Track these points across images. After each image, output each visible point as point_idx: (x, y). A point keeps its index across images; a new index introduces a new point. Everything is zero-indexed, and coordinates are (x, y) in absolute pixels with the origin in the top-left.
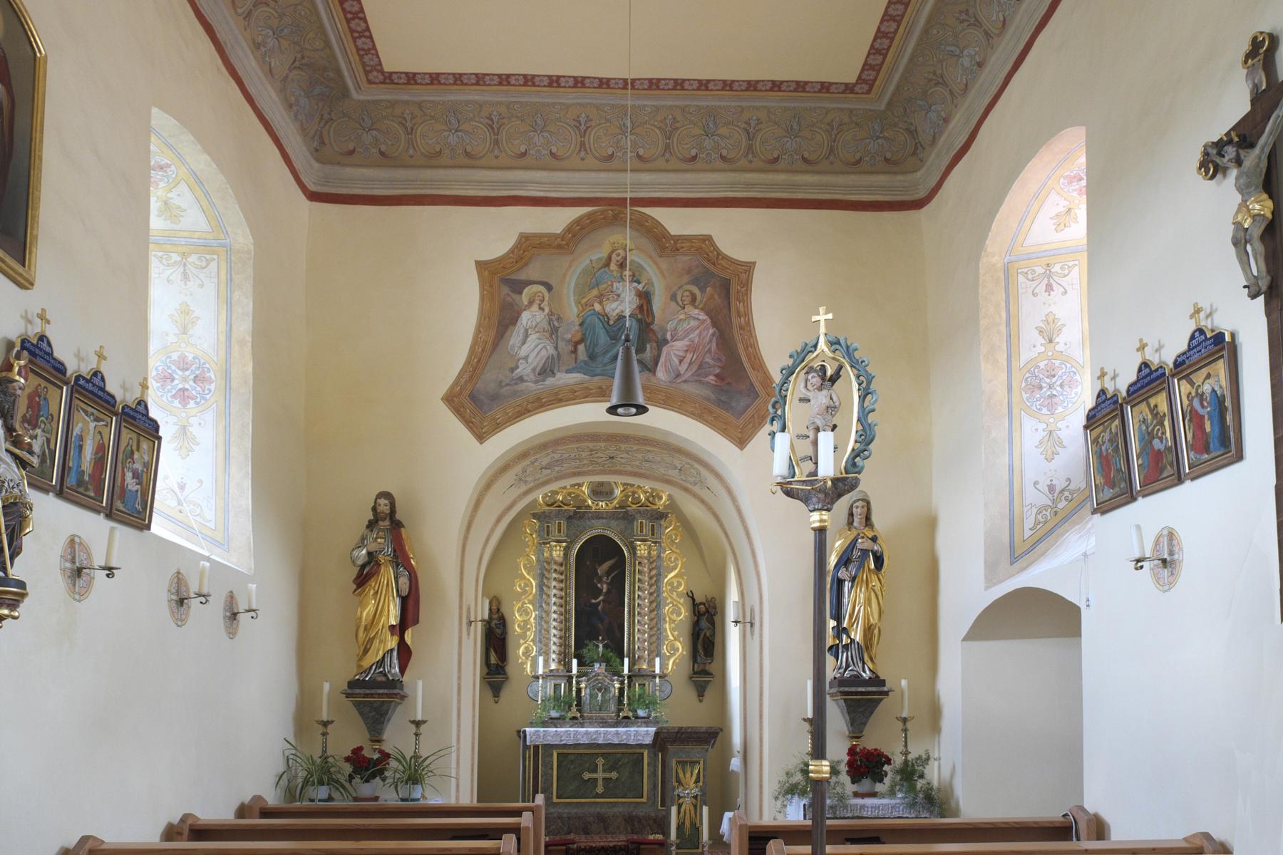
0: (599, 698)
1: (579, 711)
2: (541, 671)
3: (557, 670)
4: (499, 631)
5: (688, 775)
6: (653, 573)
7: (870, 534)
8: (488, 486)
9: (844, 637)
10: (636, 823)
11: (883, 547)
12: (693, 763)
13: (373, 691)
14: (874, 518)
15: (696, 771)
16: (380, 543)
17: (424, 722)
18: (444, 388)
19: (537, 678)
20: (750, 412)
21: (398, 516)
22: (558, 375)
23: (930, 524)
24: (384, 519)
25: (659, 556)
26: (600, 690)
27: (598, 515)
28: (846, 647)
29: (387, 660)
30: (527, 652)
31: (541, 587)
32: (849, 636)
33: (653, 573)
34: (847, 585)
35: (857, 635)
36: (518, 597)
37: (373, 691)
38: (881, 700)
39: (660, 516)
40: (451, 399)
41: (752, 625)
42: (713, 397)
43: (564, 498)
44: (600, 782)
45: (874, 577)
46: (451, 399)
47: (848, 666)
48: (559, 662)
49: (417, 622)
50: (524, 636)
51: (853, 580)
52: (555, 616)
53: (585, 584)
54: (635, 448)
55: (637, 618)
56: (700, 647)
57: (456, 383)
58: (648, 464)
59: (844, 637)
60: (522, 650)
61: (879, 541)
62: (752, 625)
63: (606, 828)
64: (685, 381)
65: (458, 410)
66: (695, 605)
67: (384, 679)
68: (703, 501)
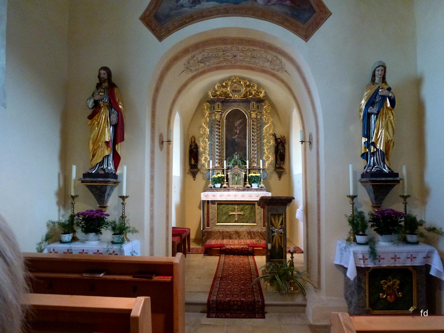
0: (236, 179)
1: (228, 184)
2: (211, 167)
3: (218, 167)
4: (195, 150)
5: (277, 221)
6: (258, 125)
7: (386, 87)
8: (167, 68)
9: (372, 148)
10: (252, 235)
11: (395, 93)
12: (279, 215)
13: (95, 179)
14: (387, 79)
15: (281, 219)
16: (102, 95)
17: (127, 197)
18: (140, 13)
19: (209, 170)
20: (310, 21)
21: (113, 80)
22: (203, 3)
23: (418, 83)
24: (104, 82)
25: (261, 118)
26: (236, 175)
27: (235, 101)
28: (373, 154)
29: (106, 161)
30: (206, 160)
31: (211, 131)
32: (375, 147)
33: (258, 125)
34: (373, 117)
35: (381, 146)
36: (202, 136)
37: (95, 179)
38: (394, 185)
39: (260, 101)
40: (145, 19)
41: (310, 143)
42: (289, 12)
43: (220, 94)
44: (236, 216)
45: (390, 112)
46: (145, 19)
47: (374, 165)
48: (219, 163)
49: (123, 140)
50: (205, 153)
51: (377, 114)
52: (217, 144)
53: (230, 129)
54: (247, 48)
55: (252, 141)
56: (278, 157)
57: (147, 9)
58: (253, 60)
59: (372, 148)
60: (203, 158)
61: (392, 90)
62: (310, 143)
63: (239, 237)
64: (274, 4)
65: (148, 25)
66: (276, 140)
67: (103, 172)
68: (283, 81)
